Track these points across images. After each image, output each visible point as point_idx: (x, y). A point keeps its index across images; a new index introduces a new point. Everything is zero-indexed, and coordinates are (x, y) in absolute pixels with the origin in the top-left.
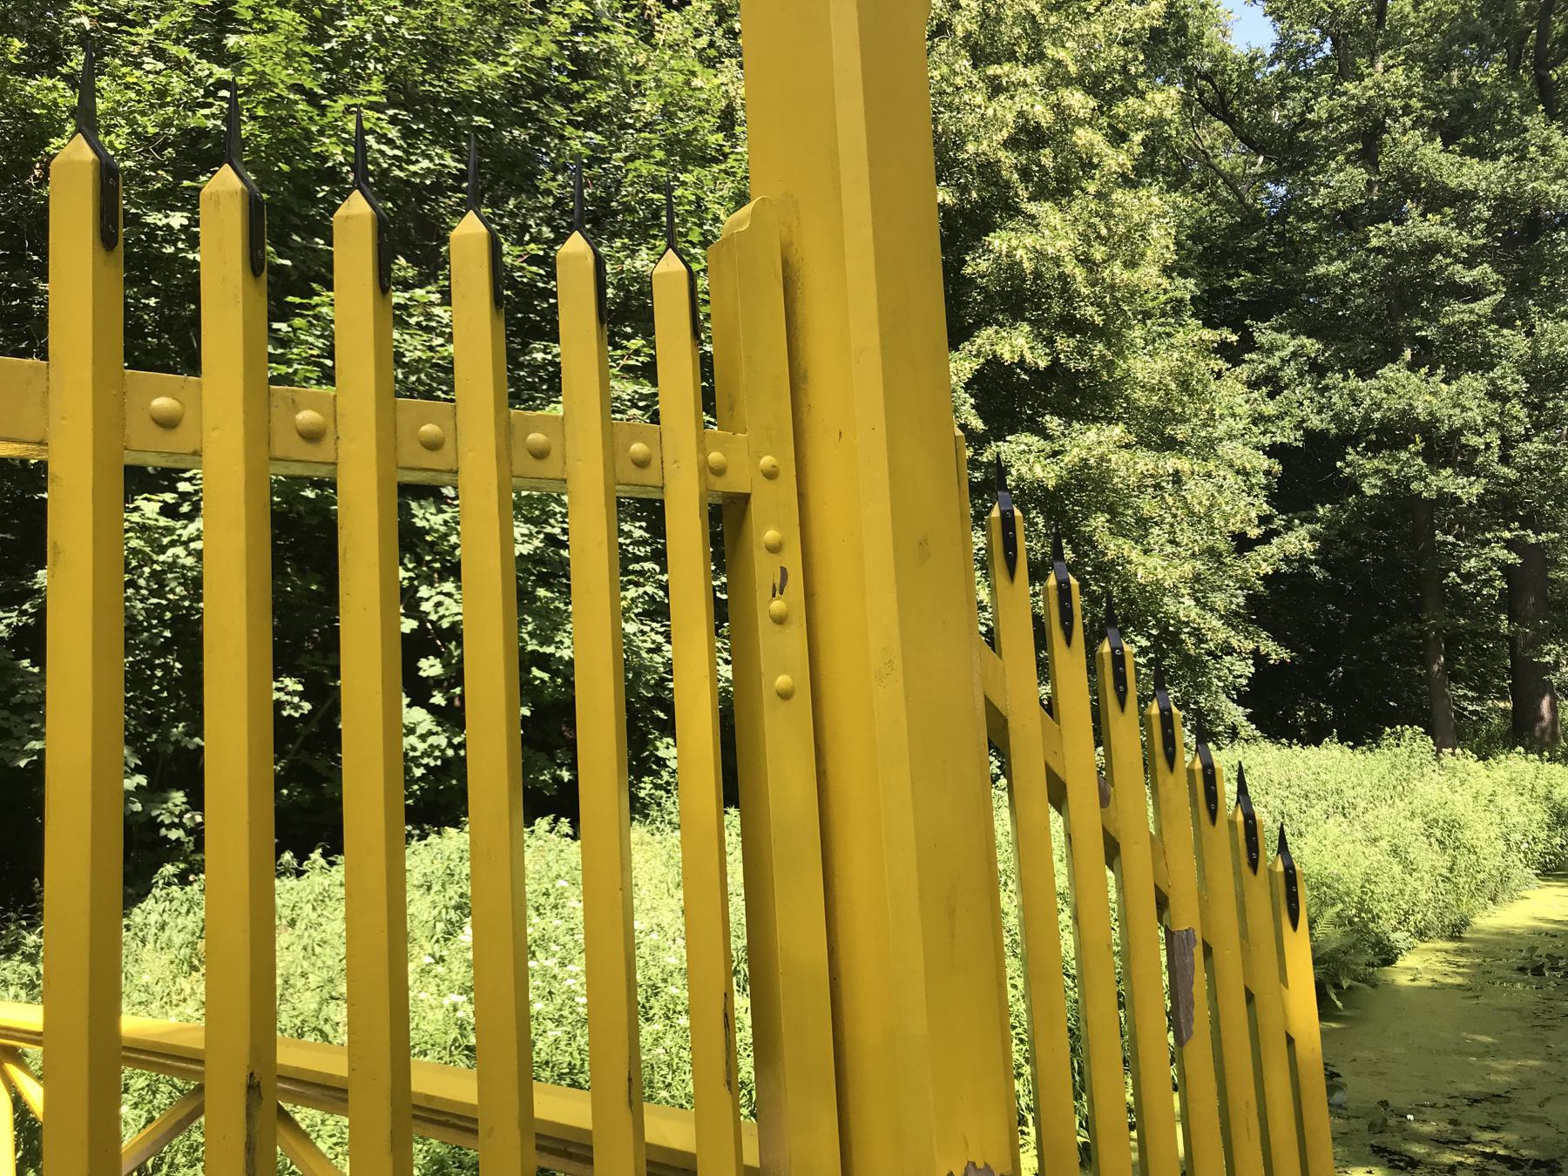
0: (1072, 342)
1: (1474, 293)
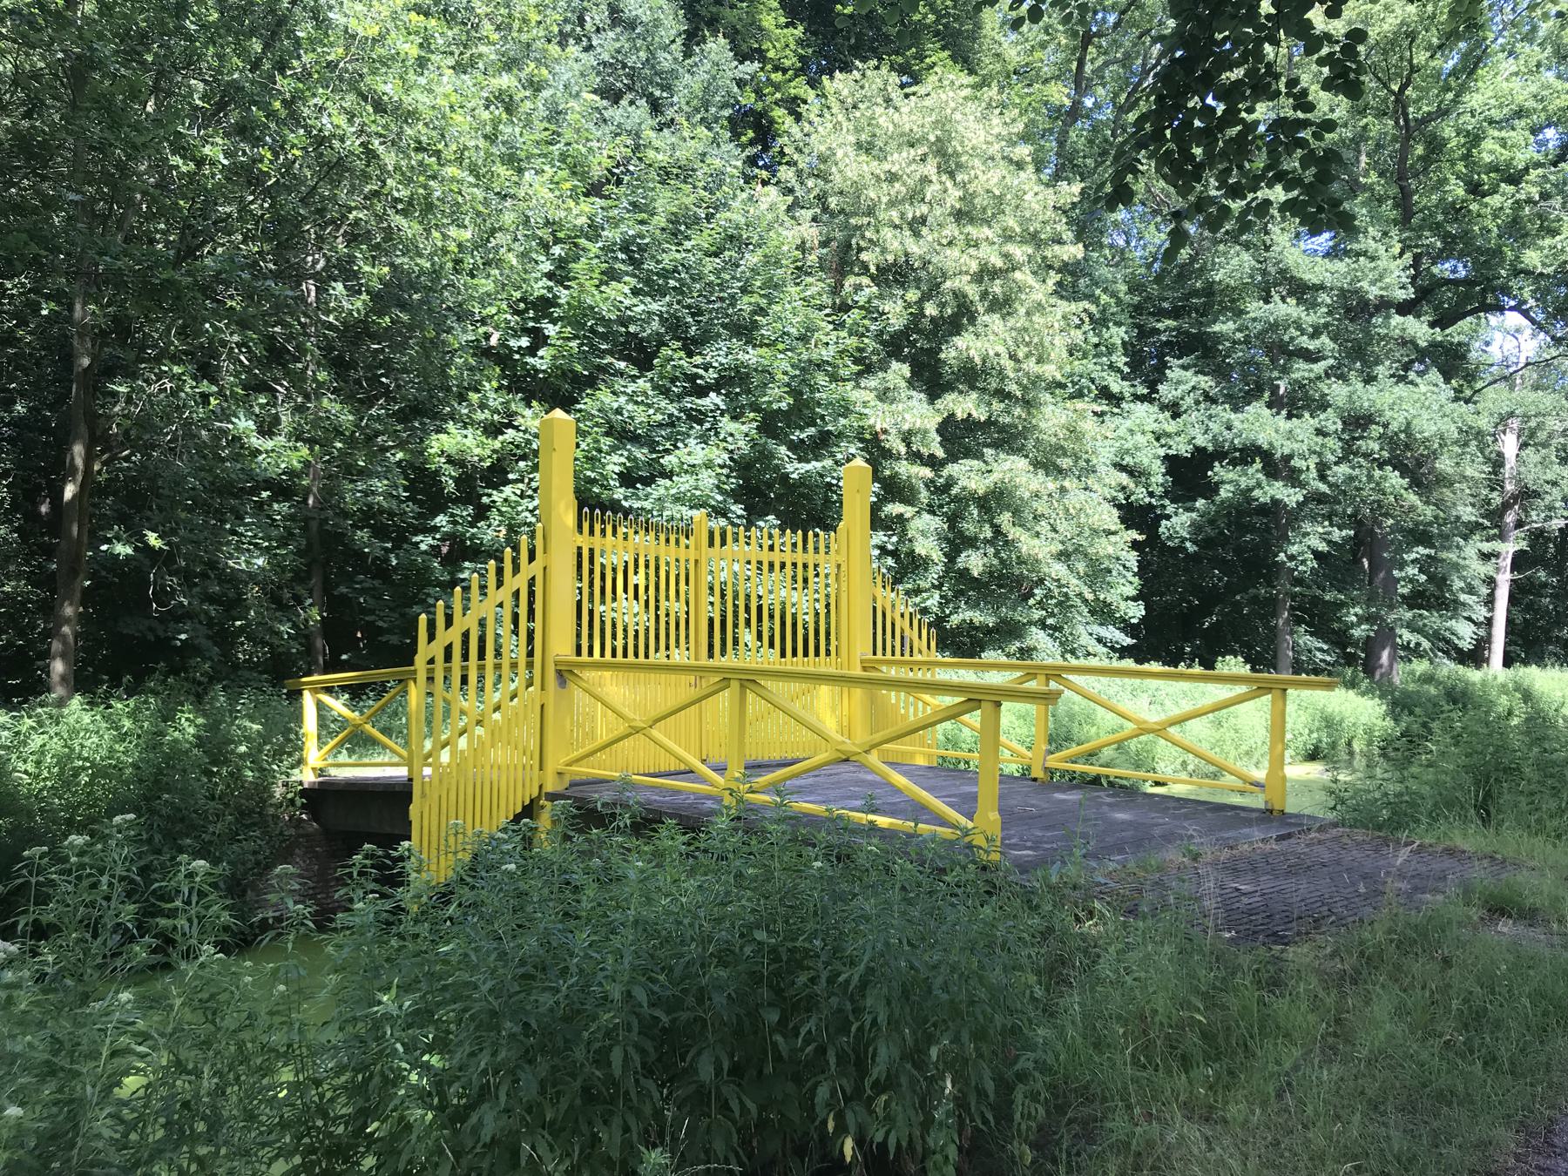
0: (1002, 405)
1: (1311, 357)
